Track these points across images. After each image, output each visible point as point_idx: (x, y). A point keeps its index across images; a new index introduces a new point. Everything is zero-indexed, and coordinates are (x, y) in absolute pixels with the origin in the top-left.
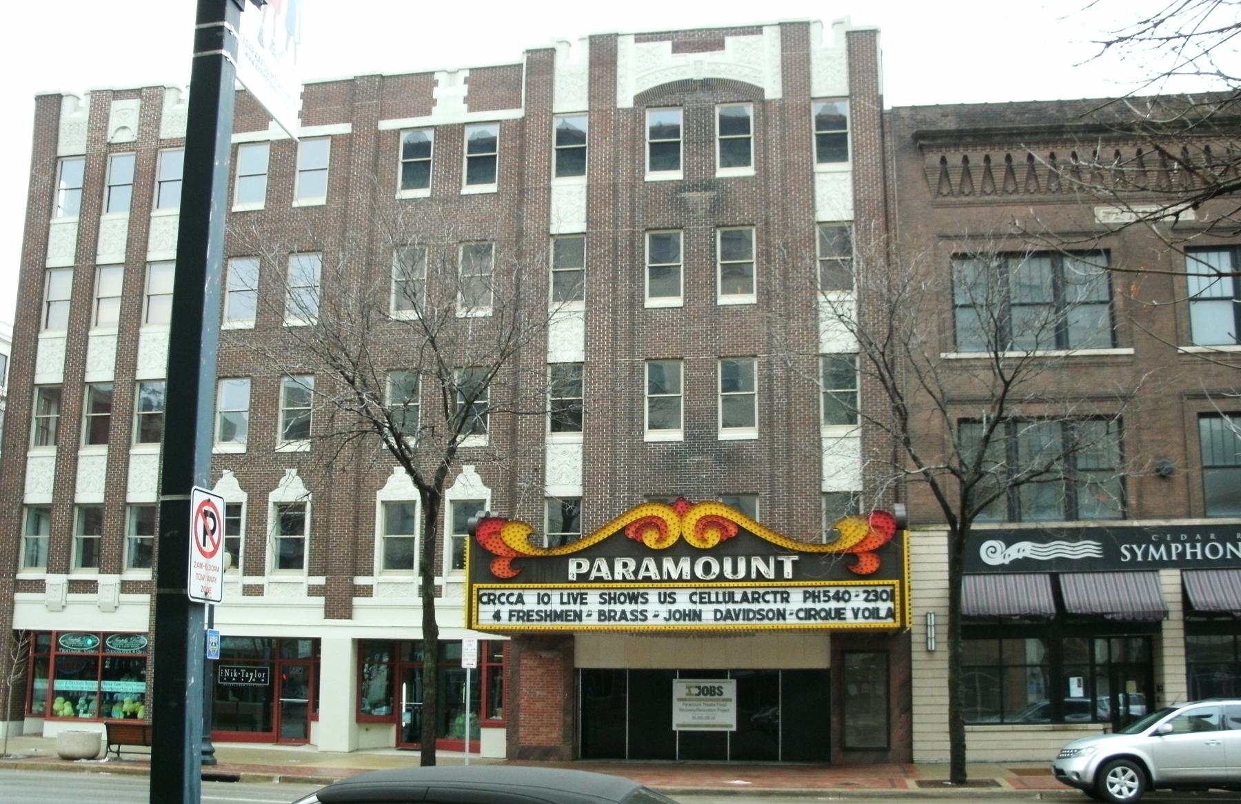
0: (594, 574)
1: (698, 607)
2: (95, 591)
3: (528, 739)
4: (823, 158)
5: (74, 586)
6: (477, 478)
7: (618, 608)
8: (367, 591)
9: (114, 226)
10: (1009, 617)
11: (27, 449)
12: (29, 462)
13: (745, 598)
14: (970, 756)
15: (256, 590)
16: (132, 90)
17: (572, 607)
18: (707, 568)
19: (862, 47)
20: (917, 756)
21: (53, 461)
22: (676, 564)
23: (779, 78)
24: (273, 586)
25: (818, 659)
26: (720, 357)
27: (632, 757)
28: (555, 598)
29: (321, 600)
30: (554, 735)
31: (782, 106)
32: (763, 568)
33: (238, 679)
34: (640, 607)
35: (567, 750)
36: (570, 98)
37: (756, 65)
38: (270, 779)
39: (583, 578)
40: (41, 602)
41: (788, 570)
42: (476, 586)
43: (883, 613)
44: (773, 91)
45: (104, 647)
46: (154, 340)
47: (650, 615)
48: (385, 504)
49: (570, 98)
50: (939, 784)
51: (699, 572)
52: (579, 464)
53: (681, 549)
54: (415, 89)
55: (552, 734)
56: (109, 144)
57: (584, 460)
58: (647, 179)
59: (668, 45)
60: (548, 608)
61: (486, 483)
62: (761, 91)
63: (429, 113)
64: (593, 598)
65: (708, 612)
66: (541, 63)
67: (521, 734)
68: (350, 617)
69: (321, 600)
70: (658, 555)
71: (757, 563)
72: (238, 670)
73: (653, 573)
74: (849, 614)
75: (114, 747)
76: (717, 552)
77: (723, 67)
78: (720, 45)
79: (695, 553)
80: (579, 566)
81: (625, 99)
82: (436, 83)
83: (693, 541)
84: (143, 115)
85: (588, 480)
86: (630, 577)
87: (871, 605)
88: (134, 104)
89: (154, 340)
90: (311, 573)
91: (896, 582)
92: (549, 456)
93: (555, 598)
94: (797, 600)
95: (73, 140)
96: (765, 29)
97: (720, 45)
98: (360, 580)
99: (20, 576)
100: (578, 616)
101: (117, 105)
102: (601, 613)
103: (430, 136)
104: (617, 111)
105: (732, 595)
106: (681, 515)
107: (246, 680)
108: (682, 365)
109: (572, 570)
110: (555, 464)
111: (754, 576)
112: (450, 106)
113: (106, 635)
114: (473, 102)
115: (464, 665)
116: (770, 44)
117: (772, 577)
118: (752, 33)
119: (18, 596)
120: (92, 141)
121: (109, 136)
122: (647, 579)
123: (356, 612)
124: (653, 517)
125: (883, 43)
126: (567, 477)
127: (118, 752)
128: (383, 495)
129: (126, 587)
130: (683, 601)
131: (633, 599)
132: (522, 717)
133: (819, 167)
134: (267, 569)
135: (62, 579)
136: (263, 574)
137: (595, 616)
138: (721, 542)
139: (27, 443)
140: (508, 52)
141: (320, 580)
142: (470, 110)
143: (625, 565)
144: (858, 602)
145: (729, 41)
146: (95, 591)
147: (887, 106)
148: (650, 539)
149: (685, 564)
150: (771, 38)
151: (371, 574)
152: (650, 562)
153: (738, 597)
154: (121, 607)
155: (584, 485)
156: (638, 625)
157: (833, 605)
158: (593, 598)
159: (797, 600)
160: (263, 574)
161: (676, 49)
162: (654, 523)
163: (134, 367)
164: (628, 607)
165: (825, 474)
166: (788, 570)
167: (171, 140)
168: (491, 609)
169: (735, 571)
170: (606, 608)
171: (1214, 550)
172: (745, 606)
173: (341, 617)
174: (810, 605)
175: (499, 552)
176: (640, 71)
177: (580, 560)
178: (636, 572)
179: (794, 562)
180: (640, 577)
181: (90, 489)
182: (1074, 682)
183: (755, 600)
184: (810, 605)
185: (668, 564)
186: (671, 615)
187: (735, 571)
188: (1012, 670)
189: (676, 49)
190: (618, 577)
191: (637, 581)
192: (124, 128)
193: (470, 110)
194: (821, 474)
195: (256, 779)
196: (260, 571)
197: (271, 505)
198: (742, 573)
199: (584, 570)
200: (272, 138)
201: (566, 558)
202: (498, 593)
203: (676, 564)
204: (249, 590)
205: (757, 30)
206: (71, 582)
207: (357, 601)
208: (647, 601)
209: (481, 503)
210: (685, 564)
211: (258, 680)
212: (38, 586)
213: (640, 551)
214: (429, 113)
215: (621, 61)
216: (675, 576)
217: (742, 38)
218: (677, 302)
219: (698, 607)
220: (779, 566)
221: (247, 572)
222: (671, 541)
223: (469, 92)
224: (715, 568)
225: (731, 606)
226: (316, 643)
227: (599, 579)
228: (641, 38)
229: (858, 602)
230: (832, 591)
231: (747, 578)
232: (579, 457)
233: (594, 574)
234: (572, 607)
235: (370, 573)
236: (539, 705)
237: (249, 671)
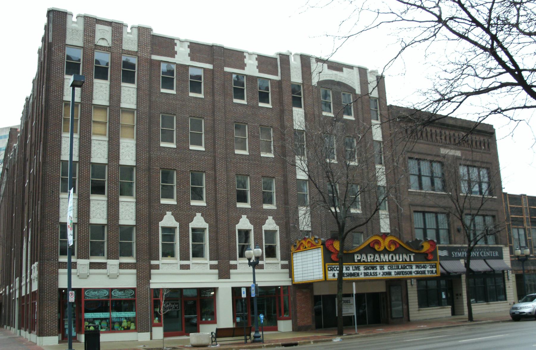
1: (390, 271)
2: (106, 268)
3: (301, 323)
4: (97, 77)
5: (93, 266)
7: (369, 271)
8: (157, 267)
9: (101, 87)
10: (480, 272)
13: (402, 268)
14: (473, 312)
15: (187, 267)
16: (106, 21)
17: (356, 271)
20: (411, 319)
24: (194, 265)
25: (381, 289)
26: (161, 168)
27: (369, 323)
28: (351, 268)
30: (309, 321)
34: (375, 271)
35: (314, 326)
37: (352, 79)
38: (309, 342)
39: (359, 261)
42: (327, 264)
43: (434, 272)
44: (358, 91)
46: (128, 146)
47: (378, 274)
50: (466, 322)
51: (390, 258)
53: (386, 251)
54: (237, 57)
55: (309, 320)
56: (96, 45)
60: (349, 272)
61: (206, 221)
64: (362, 268)
65: (393, 272)
67: (298, 322)
68: (230, 278)
69: (216, 271)
70: (379, 253)
71: (405, 256)
73: (378, 260)
74: (427, 272)
76: (395, 252)
77: (343, 78)
78: (341, 70)
79: (389, 252)
86: (372, 261)
87: (431, 269)
88: (109, 29)
89: (128, 146)
93: (351, 268)
94: (414, 269)
96: (354, 68)
98: (153, 262)
100: (358, 274)
102: (365, 273)
103: (174, 67)
104: (312, 86)
105: (398, 266)
106: (384, 239)
108: (274, 180)
112: (251, 68)
113: (112, 289)
120: (86, 41)
121: (96, 41)
122: (377, 261)
123: (231, 276)
124: (376, 240)
126: (100, 215)
128: (162, 224)
129: (122, 266)
130: (386, 270)
131: (373, 268)
132: (298, 315)
133: (123, 84)
136: (189, 260)
137: (363, 274)
138: (395, 249)
140: (271, 52)
141: (215, 262)
143: (371, 257)
144: (428, 269)
147: (388, 104)
148: (376, 247)
149: (386, 256)
152: (377, 256)
153: (400, 267)
154: (90, 276)
156: (375, 277)
157: (423, 269)
158: (362, 268)
159: (414, 269)
160: (189, 260)
163: (118, 158)
164: (372, 271)
167: (128, 51)
168: (332, 272)
169: (399, 259)
170: (366, 271)
171: (483, 254)
172: (402, 270)
173: (226, 278)
174: (417, 270)
175: (332, 251)
177: (358, 255)
179: (414, 256)
182: (443, 293)
183: (404, 268)
184: (417, 270)
185: (382, 256)
186: (384, 273)
190: (369, 261)
191: (374, 262)
192: (103, 39)
193: (260, 72)
194: (118, 217)
195: (304, 343)
198: (401, 260)
199: (359, 258)
200: (177, 62)
202: (333, 267)
204: (183, 267)
205: (351, 67)
206: (91, 263)
207: (232, 271)
208: (376, 269)
210: (386, 256)
213: (375, 252)
216: (384, 260)
218: (173, 146)
219: (390, 271)
221: (181, 259)
222: (382, 248)
223: (258, 64)
224: (394, 258)
225: (399, 270)
227: (364, 261)
228: (318, 60)
229: (428, 269)
230: (422, 265)
231: (403, 261)
234: (356, 271)
235: (158, 259)
236: (303, 310)
237: (173, 304)
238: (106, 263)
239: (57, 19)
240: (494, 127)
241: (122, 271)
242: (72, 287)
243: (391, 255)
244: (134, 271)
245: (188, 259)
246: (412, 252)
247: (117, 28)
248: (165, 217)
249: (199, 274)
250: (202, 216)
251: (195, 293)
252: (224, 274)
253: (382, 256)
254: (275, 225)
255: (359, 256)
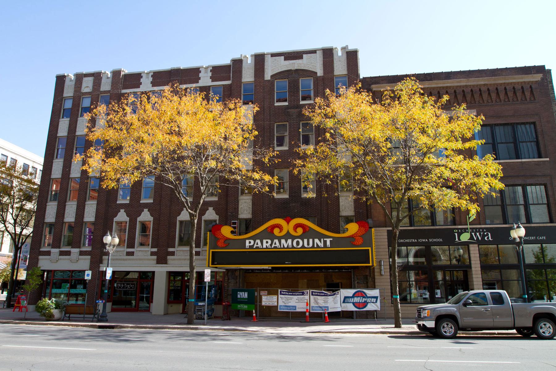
0: (255, 246)
2: (70, 255)
5: (62, 253)
6: (214, 212)
8: (173, 254)
11: (47, 202)
12: (47, 207)
15: (132, 254)
18: (298, 243)
19: (352, 57)
21: (56, 206)
22: (286, 242)
23: (322, 68)
29: (155, 257)
31: (323, 78)
32: (319, 244)
33: (123, 287)
36: (248, 76)
40: (69, 259)
41: (328, 243)
42: (211, 251)
44: (320, 73)
45: (72, 276)
48: (205, 221)
49: (248, 76)
51: (295, 244)
52: (251, 206)
53: (288, 236)
57: (253, 205)
58: (275, 105)
59: (283, 57)
61: (152, 215)
62: (316, 73)
63: (198, 82)
66: (238, 63)
69: (155, 257)
71: (317, 241)
72: (124, 284)
75: (68, 315)
76: (302, 237)
78: (301, 58)
79: (293, 238)
80: (250, 243)
81: (268, 77)
82: (200, 72)
83: (293, 233)
84: (94, 83)
85: (254, 212)
88: (91, 79)
90: (152, 247)
91: (370, 248)
92: (240, 204)
95: (69, 92)
96: (317, 52)
97: (301, 58)
98: (171, 250)
99: (41, 250)
101: (85, 79)
106: (288, 223)
107: (127, 288)
109: (247, 244)
110: (242, 206)
111: (315, 246)
114: (213, 79)
115: (205, 280)
116: (319, 57)
117: (322, 246)
118: (313, 53)
119: (40, 257)
123: (169, 262)
125: (360, 56)
127: (69, 317)
128: (180, 218)
129: (82, 253)
134: (136, 246)
135: (57, 250)
139: (47, 200)
141: (155, 250)
142: (212, 81)
143: (267, 242)
145: (304, 56)
146: (70, 255)
147: (361, 77)
149: (290, 241)
150: (319, 55)
151: (174, 247)
152: (276, 241)
155: (252, 214)
161: (285, 59)
162: (279, 227)
165: (341, 210)
166: (328, 243)
169: (308, 244)
176: (272, 68)
178: (271, 245)
180: (273, 247)
181: (70, 216)
185: (283, 241)
187: (308, 244)
188: (512, 282)
189: (285, 59)
190: (264, 246)
196: (133, 247)
197: (138, 223)
198: (311, 245)
201: (245, 240)
203: (286, 242)
204: (128, 254)
205: (314, 52)
206: (60, 251)
207: (169, 257)
209: (215, 221)
211: (131, 288)
212: (48, 253)
213: (272, 237)
214: (198, 82)
215: (266, 64)
216: (286, 246)
217: (309, 55)
220: (325, 242)
221: (128, 247)
222: (284, 233)
226: (153, 273)
228: (273, 55)
232: (251, 204)
233: (255, 246)
237: (128, 284)
238: (50, 251)
239: (61, 80)
240: (547, 68)
241: (81, 257)
242: (531, 325)
243: (295, 241)
244: (89, 257)
245: (133, 247)
246: (328, 237)
247: (97, 77)
248: (119, 213)
249: (142, 260)
250: (148, 211)
251: (136, 276)
252: (162, 260)
253: (283, 241)
254: (215, 214)
255: (252, 242)
